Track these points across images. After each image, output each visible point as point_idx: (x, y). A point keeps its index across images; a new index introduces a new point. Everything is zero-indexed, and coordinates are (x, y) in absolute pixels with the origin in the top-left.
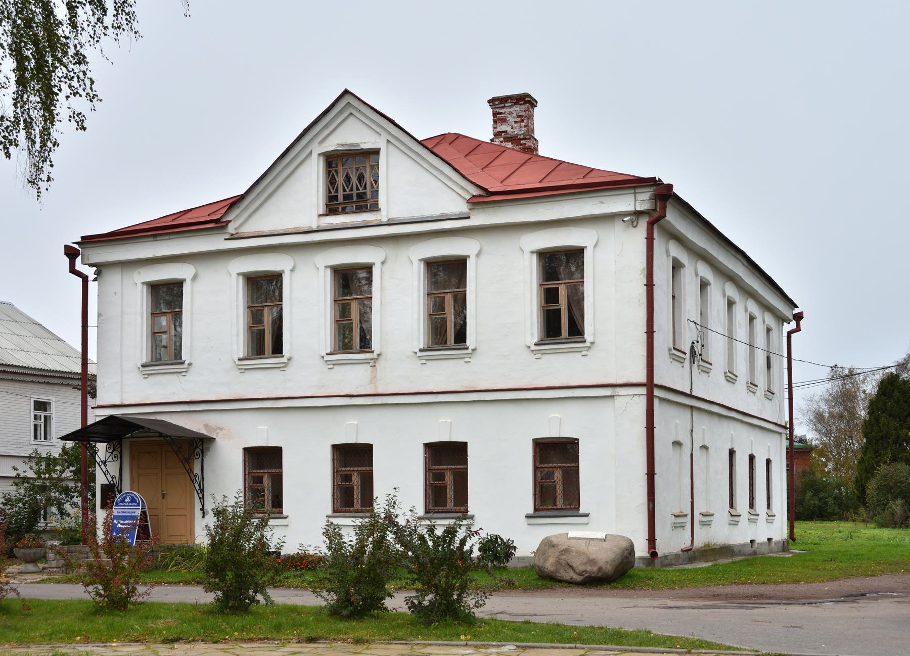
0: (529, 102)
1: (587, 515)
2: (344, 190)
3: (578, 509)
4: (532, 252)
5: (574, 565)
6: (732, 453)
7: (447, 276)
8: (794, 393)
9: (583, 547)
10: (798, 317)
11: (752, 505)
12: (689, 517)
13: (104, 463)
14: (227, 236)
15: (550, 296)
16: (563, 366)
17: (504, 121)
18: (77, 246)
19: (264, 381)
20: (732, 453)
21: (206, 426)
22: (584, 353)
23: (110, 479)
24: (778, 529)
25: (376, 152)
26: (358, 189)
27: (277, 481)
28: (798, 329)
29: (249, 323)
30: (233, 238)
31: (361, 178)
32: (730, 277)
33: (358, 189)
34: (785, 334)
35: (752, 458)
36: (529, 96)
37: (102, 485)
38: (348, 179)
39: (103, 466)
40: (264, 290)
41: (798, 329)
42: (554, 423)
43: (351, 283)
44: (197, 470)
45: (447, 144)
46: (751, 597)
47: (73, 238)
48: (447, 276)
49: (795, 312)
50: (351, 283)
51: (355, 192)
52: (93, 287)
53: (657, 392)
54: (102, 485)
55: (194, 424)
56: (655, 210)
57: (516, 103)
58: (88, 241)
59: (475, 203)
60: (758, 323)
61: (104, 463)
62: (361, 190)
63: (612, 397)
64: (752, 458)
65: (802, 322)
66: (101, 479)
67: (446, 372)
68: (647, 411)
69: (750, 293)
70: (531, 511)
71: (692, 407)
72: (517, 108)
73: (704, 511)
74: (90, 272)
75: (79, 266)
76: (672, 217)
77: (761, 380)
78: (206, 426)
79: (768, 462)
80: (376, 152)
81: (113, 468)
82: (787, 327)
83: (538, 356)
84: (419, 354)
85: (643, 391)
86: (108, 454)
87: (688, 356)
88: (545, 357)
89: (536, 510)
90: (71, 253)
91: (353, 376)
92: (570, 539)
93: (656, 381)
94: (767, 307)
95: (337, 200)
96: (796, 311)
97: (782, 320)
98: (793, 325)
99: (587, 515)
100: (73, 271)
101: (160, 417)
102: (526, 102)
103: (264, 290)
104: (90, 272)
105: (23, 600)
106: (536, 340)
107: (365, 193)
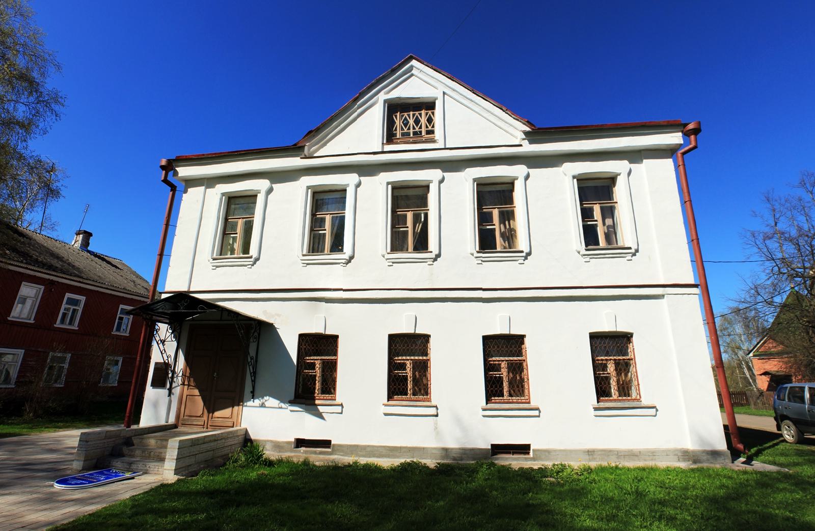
2: (427, 127)
6: (386, 414)
7: (494, 198)
13: (163, 342)
14: (303, 156)
19: (328, 274)
20: (386, 414)
21: (265, 312)
22: (628, 258)
23: (166, 358)
25: (430, 105)
30: (306, 158)
37: (156, 364)
38: (406, 123)
39: (161, 345)
40: (326, 204)
43: (408, 201)
44: (252, 352)
45: (299, 158)
48: (494, 198)
50: (408, 201)
54: (156, 364)
61: (163, 342)
66: (156, 357)
67: (498, 272)
78: (265, 312)
80: (430, 105)
81: (171, 346)
83: (588, 259)
86: (168, 334)
91: (412, 272)
95: (410, 135)
103: (326, 204)
107: (421, 132)
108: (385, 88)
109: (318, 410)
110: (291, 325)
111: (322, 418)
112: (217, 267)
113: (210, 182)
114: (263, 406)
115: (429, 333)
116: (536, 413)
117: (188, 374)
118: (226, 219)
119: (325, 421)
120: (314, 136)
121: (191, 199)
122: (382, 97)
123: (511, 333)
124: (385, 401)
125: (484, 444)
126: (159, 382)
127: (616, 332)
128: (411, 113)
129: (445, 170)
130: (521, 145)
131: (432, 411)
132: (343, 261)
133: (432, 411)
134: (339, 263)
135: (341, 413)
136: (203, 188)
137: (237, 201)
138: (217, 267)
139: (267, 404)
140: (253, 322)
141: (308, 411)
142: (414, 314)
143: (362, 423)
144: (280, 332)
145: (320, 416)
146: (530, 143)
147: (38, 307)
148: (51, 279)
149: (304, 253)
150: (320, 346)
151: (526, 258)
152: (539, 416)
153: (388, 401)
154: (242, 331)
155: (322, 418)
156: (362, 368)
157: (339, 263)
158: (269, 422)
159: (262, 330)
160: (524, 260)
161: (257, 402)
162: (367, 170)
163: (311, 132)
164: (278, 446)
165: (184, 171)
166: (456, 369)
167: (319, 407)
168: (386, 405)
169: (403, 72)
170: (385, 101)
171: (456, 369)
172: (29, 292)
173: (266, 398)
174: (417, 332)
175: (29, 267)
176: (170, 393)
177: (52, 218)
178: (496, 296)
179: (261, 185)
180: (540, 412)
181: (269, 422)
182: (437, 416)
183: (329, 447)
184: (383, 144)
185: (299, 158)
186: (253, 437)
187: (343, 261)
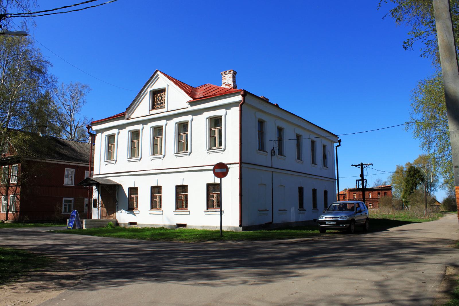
0: (76, 153)
7: (183, 127)
10: (340, 141)
20: (150, 214)
24: (16, 182)
26: (161, 101)
28: (340, 145)
31: (162, 98)
33: (161, 101)
34: (335, 147)
40: (135, 135)
41: (340, 145)
43: (158, 131)
46: (437, 242)
48: (183, 127)
49: (338, 140)
50: (158, 131)
51: (160, 102)
59: (191, 103)
65: (341, 143)
68: (195, 172)
82: (336, 144)
93: (242, 162)
96: (339, 139)
98: (338, 144)
105: (396, 172)
108: (154, 80)
109: (134, 213)
110: (126, 183)
111: (135, 215)
112: (106, 164)
113: (102, 131)
114: (121, 213)
115: (161, 186)
116: (188, 213)
117: (102, 203)
118: (109, 145)
119: (135, 216)
120: (129, 110)
121: (98, 137)
122: (149, 89)
123: (215, 182)
124: (150, 210)
125: (174, 223)
126: (95, 206)
127: (214, 183)
128: (160, 94)
129: (167, 120)
130: (188, 108)
131: (161, 213)
132: (139, 160)
133: (161, 213)
134: (137, 161)
135: (139, 214)
136: (101, 133)
137: (111, 137)
138: (106, 164)
139: (122, 212)
140: (103, 185)
141: (131, 213)
142: (157, 179)
143: (144, 217)
144: (123, 187)
145: (134, 214)
146: (191, 106)
147: (74, 179)
148: (77, 165)
149: (129, 158)
150: (134, 190)
151: (190, 155)
152: (189, 214)
153: (151, 209)
154: (108, 188)
155: (135, 215)
156: (144, 198)
157: (137, 161)
158: (123, 217)
159: (118, 187)
160: (189, 156)
161: (120, 211)
162: (144, 122)
163: (127, 109)
164: (125, 224)
165: (95, 128)
166: (169, 197)
167: (134, 212)
168: (150, 211)
169: (155, 77)
170: (150, 91)
171: (169, 197)
172: (68, 172)
173: (122, 210)
174: (135, 187)
175: (66, 161)
176: (98, 210)
177: (88, 118)
178: (170, 171)
179: (115, 131)
180: (190, 213)
181: (123, 217)
182: (163, 214)
183: (136, 225)
184: (150, 110)
185: (124, 120)
186: (119, 222)
187: (139, 160)
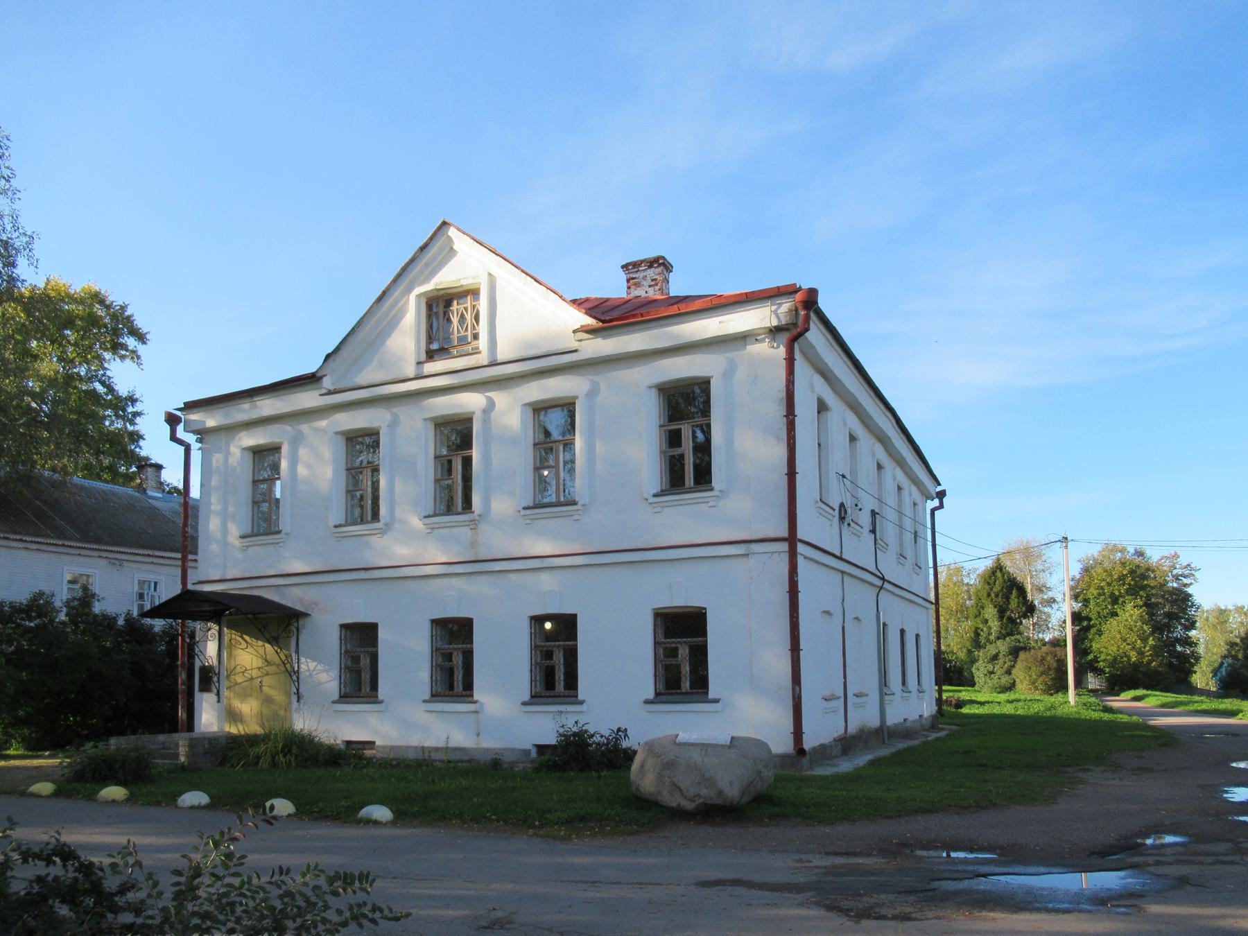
0: (663, 264)
1: (716, 701)
3: (707, 693)
4: (650, 387)
5: (682, 786)
8: (788, 669)
9: (696, 756)
10: (941, 495)
11: (904, 683)
12: (842, 699)
14: (324, 391)
15: (674, 439)
16: (686, 520)
17: (638, 285)
18: (178, 413)
27: (468, 656)
28: (941, 506)
29: (347, 485)
30: (330, 393)
32: (883, 439)
34: (928, 512)
35: (902, 632)
36: (663, 258)
42: (681, 593)
47: (174, 404)
52: (196, 457)
53: (801, 548)
55: (291, 598)
56: (795, 325)
57: (651, 266)
58: (190, 406)
60: (905, 493)
62: (463, 333)
63: (746, 555)
64: (902, 632)
65: (945, 500)
69: (900, 462)
70: (650, 695)
71: (843, 572)
72: (651, 273)
73: (857, 691)
74: (190, 438)
75: (181, 433)
76: (815, 335)
77: (909, 553)
79: (917, 636)
83: (658, 509)
84: (523, 512)
85: (785, 546)
87: (837, 513)
88: (667, 510)
89: (657, 694)
90: (172, 420)
92: (679, 744)
94: (915, 481)
96: (939, 489)
97: (929, 497)
98: (936, 503)
99: (716, 701)
100: (174, 438)
101: (256, 593)
102: (660, 265)
104: (190, 438)
106: (656, 488)
